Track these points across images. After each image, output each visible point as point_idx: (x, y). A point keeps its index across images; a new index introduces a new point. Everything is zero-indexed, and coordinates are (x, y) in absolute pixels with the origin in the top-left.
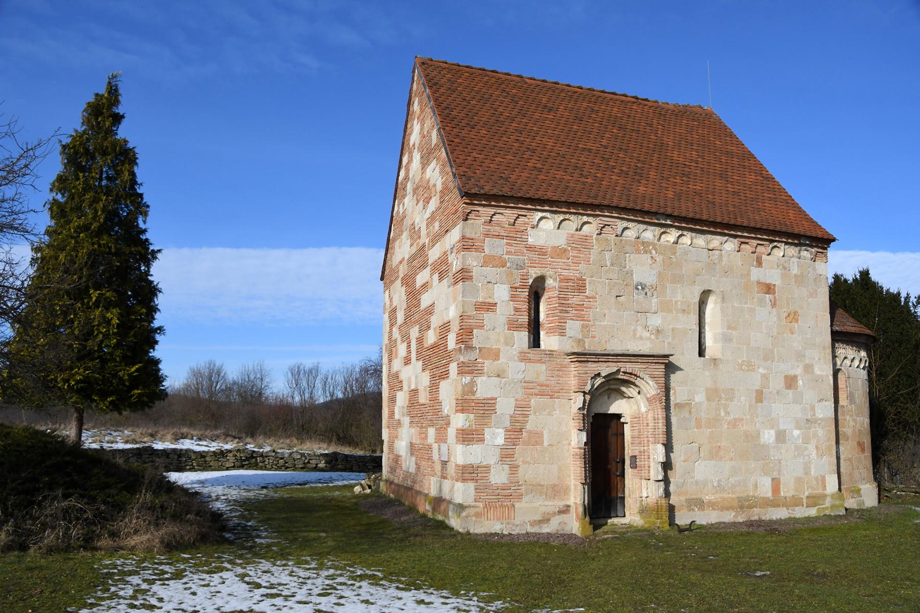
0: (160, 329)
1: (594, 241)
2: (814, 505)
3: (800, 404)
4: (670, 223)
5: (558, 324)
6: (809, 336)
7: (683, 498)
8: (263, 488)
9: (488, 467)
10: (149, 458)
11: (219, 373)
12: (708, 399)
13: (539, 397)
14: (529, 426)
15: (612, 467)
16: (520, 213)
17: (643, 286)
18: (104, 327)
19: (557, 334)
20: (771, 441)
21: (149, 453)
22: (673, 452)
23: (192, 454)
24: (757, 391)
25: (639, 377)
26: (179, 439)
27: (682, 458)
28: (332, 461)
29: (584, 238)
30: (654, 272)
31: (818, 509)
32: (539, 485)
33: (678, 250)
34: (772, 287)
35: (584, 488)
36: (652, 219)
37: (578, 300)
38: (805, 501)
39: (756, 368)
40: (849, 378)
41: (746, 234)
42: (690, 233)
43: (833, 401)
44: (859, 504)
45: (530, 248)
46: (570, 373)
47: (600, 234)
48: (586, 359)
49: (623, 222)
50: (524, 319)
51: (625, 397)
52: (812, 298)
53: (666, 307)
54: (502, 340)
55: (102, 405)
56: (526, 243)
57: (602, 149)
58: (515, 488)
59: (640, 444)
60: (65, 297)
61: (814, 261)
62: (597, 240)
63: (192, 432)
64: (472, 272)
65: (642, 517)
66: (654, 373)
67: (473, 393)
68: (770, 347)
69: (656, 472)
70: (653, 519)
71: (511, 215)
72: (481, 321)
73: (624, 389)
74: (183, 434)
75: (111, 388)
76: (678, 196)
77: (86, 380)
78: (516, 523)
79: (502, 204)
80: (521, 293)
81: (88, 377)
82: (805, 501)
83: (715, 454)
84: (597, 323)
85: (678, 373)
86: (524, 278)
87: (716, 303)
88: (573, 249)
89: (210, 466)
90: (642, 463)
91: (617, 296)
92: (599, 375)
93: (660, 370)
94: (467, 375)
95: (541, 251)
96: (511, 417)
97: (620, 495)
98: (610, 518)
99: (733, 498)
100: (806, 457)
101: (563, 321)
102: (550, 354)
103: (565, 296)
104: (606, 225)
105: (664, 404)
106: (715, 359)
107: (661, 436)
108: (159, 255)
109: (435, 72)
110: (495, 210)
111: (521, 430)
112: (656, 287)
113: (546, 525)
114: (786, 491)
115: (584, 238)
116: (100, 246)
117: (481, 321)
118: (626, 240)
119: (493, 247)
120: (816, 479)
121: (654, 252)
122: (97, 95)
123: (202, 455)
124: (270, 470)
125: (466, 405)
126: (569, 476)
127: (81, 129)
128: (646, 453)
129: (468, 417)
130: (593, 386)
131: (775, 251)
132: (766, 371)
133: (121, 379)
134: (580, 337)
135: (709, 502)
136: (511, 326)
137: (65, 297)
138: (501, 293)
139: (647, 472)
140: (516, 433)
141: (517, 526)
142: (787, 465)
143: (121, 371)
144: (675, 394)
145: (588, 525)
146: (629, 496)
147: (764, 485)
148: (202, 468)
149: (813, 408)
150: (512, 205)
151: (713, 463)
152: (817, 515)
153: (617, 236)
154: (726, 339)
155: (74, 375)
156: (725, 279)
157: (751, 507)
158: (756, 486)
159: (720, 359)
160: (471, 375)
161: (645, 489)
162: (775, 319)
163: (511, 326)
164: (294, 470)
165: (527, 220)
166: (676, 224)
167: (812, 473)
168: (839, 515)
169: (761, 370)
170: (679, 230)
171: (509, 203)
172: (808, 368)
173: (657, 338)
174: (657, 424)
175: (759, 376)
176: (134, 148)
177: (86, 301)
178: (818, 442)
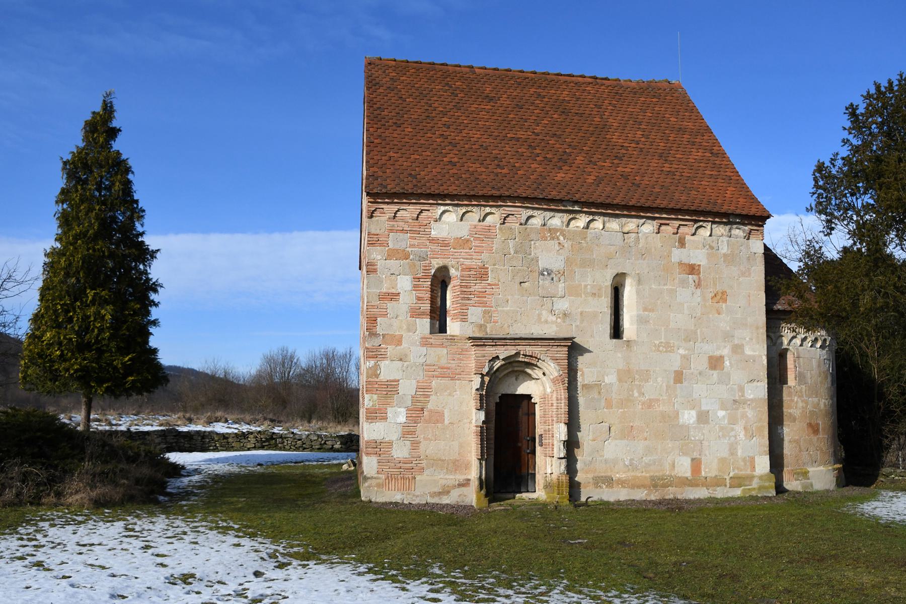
0: (155, 323)
1: (498, 231)
2: (740, 486)
3: (727, 385)
4: (578, 209)
5: (460, 311)
6: (739, 316)
7: (590, 476)
8: (259, 465)
9: (391, 443)
10: (173, 439)
11: (292, 357)
12: (620, 380)
13: (440, 379)
14: (430, 406)
15: (523, 445)
16: (422, 208)
17: (550, 272)
18: (99, 322)
19: (459, 320)
20: (691, 422)
21: (175, 434)
22: (580, 431)
23: (215, 436)
24: (676, 372)
25: (539, 359)
26: (212, 423)
27: (591, 437)
28: (347, 442)
29: (487, 228)
30: (562, 258)
31: (743, 490)
32: (440, 460)
33: (588, 235)
34: (697, 268)
35: (481, 464)
36: (559, 206)
37: (480, 287)
38: (728, 481)
39: (675, 349)
40: (798, 357)
41: (664, 216)
42: (602, 218)
43: (766, 381)
44: (804, 486)
45: (433, 241)
46: (471, 356)
47: (504, 223)
48: (483, 343)
49: (528, 211)
50: (427, 307)
51: (534, 379)
52: (744, 277)
53: (573, 291)
54: (405, 327)
55: (99, 391)
56: (428, 236)
57: (533, 137)
58: (416, 462)
59: (545, 423)
60: (67, 297)
61: (748, 239)
62: (500, 229)
63: (226, 416)
64: (377, 265)
65: (547, 493)
66: (556, 355)
67: (377, 376)
68: (693, 328)
69: (560, 451)
70: (555, 494)
71: (414, 210)
72: (385, 310)
73: (529, 371)
74: (216, 418)
75: (107, 376)
76: (599, 181)
77: (83, 369)
78: (416, 494)
79: (404, 201)
80: (424, 283)
81: (86, 366)
82: (728, 481)
83: (628, 433)
84: (499, 309)
85: (587, 355)
86: (426, 269)
87: (631, 285)
88: (476, 239)
89: (233, 447)
90: (547, 441)
91: (521, 283)
92: (497, 357)
93: (562, 353)
94: (371, 359)
95: (443, 243)
96: (412, 397)
97: (530, 472)
98: (521, 492)
99: (645, 477)
100: (733, 439)
101: (464, 308)
102: (451, 339)
103: (466, 284)
104: (509, 214)
105: (567, 385)
106: (629, 341)
107: (563, 416)
108: (158, 255)
109: (380, 72)
110: (399, 207)
111: (422, 409)
112: (564, 273)
113: (446, 497)
114: (709, 470)
115: (487, 228)
116: (94, 250)
117: (385, 310)
118: (531, 228)
119: (396, 241)
120: (744, 460)
121: (561, 238)
122: (94, 113)
123: (224, 436)
124: (289, 450)
125: (370, 386)
126: (470, 452)
127: (81, 144)
128: (551, 432)
129: (372, 397)
130: (491, 368)
131: (701, 231)
132: (687, 352)
133: (115, 368)
134: (482, 323)
135: (619, 479)
136: (414, 314)
137: (67, 297)
138: (404, 283)
139: (551, 449)
140: (418, 412)
141: (417, 496)
142: (709, 446)
143: (115, 360)
144: (582, 375)
145: (483, 498)
146: (538, 472)
147: (682, 464)
148: (225, 449)
149: (741, 389)
150: (414, 201)
151: (625, 442)
152: (742, 495)
153: (521, 224)
154: (641, 321)
155: (73, 365)
156: (640, 261)
157: (665, 486)
158: (673, 466)
159: (635, 340)
160: (374, 359)
161: (550, 466)
162: (699, 299)
163: (414, 314)
164: (311, 451)
165: (430, 214)
166: (585, 209)
167: (739, 454)
168: (768, 497)
169: (681, 351)
170: (590, 215)
171: (411, 200)
172: (737, 349)
173: (564, 322)
174: (559, 405)
175: (679, 357)
176: (127, 159)
177: (84, 300)
178: (746, 423)
